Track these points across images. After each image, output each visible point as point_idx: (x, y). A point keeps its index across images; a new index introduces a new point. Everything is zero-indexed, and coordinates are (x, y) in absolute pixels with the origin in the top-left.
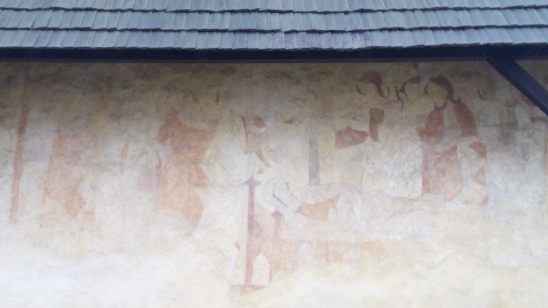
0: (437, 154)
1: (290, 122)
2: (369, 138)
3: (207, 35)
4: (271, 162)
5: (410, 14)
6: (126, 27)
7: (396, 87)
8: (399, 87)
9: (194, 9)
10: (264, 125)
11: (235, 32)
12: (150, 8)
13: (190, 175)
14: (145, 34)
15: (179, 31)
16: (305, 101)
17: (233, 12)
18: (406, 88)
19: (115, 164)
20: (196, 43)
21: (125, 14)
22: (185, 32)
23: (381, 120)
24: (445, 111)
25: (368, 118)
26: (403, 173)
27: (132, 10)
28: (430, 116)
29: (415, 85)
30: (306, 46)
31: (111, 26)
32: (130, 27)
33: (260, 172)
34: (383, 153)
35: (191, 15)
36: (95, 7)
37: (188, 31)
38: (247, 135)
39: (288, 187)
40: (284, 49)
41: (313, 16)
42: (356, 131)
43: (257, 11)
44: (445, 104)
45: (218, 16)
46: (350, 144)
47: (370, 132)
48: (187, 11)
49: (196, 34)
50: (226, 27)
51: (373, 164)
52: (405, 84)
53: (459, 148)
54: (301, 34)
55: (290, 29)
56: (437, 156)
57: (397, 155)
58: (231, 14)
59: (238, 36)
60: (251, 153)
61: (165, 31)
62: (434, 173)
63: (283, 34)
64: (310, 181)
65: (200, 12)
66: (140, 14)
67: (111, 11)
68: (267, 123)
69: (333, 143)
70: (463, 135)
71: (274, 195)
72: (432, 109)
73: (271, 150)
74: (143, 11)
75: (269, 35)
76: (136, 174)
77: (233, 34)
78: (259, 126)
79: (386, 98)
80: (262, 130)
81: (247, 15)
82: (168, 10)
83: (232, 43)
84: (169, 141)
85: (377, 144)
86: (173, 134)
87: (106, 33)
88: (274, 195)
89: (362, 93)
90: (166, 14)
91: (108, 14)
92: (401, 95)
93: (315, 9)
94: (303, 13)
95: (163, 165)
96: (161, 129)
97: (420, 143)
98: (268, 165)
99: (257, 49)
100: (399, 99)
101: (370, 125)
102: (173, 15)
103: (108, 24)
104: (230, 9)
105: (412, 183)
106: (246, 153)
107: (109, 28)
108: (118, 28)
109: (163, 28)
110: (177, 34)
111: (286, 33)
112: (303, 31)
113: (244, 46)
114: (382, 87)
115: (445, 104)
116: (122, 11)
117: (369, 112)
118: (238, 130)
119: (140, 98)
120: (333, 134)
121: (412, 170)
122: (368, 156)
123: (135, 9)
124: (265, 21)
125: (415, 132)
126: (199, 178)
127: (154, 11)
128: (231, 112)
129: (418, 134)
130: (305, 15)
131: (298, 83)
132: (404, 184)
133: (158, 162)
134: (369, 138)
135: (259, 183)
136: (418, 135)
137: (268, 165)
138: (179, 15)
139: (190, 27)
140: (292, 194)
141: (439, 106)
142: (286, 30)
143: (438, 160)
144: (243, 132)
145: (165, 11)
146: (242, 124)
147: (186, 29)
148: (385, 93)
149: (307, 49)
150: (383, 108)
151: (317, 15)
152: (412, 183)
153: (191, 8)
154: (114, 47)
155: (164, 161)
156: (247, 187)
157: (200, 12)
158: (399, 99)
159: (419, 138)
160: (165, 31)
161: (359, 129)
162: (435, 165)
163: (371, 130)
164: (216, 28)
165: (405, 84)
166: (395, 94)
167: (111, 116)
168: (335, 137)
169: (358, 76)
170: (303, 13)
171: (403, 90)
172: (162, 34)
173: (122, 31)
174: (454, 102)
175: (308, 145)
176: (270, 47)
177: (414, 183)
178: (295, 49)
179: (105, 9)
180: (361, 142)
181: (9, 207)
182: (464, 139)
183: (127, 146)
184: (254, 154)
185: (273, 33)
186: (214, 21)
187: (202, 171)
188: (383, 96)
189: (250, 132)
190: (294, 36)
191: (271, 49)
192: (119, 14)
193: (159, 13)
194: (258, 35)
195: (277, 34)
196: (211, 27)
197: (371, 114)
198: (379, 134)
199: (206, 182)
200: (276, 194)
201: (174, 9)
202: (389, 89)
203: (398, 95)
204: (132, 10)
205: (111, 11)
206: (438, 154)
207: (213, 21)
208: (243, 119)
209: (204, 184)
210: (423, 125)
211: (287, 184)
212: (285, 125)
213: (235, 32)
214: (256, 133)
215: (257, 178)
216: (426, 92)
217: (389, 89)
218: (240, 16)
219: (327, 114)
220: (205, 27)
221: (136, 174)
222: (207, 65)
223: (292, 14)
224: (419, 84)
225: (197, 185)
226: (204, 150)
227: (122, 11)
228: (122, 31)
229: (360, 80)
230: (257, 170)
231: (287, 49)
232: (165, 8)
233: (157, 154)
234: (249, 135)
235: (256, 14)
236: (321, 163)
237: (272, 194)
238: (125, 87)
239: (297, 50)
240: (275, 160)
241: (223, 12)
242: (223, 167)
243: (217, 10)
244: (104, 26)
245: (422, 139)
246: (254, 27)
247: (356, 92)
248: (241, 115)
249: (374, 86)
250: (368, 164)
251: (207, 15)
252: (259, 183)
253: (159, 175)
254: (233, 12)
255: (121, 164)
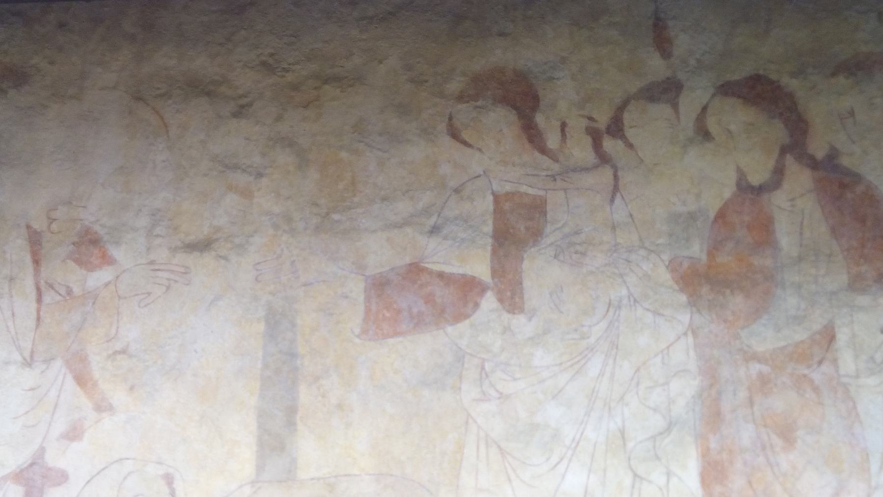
0: (755, 357)
1: (202, 246)
2: (489, 302)
4: (118, 396)
7: (591, 119)
8: (603, 120)
10: (107, 260)
16: (260, 175)
18: (628, 118)
23: (536, 234)
24: (779, 199)
25: (489, 228)
26: (622, 432)
28: (721, 216)
29: (661, 110)
33: (74, 434)
34: (541, 358)
38: (39, 300)
42: (441, 275)
44: (779, 173)
46: (418, 323)
47: (493, 277)
51: (503, 397)
52: (622, 108)
53: (842, 337)
56: (756, 368)
57: (595, 365)
62: (746, 434)
64: (260, 468)
68: (117, 253)
69: (354, 320)
70: (856, 284)
72: (728, 193)
78: (82, 262)
79: (556, 160)
80: (100, 277)
85: (518, 321)
89: (465, 143)
92: (609, 144)
97: (685, 317)
98: (103, 407)
100: (603, 158)
101: (494, 252)
105: (658, 477)
114: (540, 119)
115: (779, 173)
117: (491, 208)
120: (356, 288)
121: (657, 422)
122: (483, 368)
125: (664, 275)
129: (677, 282)
132: (628, 481)
134: (489, 302)
136: (676, 287)
137: (103, 407)
141: (756, 179)
143: (764, 384)
146: (28, 258)
148: (552, 141)
150: (541, 193)
152: (658, 477)
158: (603, 158)
159: (683, 298)
161: (454, 268)
162: (751, 402)
163: (497, 272)
165: (622, 108)
166: (588, 141)
168: (361, 298)
169: (454, 86)
171: (616, 129)
174: (814, 164)
175: (261, 327)
177: (669, 474)
180: (459, 317)
181: (34, 327)
182: (863, 300)
188: (543, 150)
189: (51, 286)
197: (498, 212)
198: (527, 283)
202: (563, 126)
203: (597, 145)
206: (759, 361)
208: (35, 241)
210: (697, 250)
212: (181, 258)
214: (77, 291)
215: (54, 459)
216: (704, 134)
217: (563, 126)
219: (336, 217)
224: (675, 106)
229: (461, 98)
230: (60, 426)
234: (47, 298)
236: (305, 395)
245: (694, 302)
247: (446, 140)
248: (28, 227)
249: (513, 116)
250: (484, 398)
252: (62, 477)
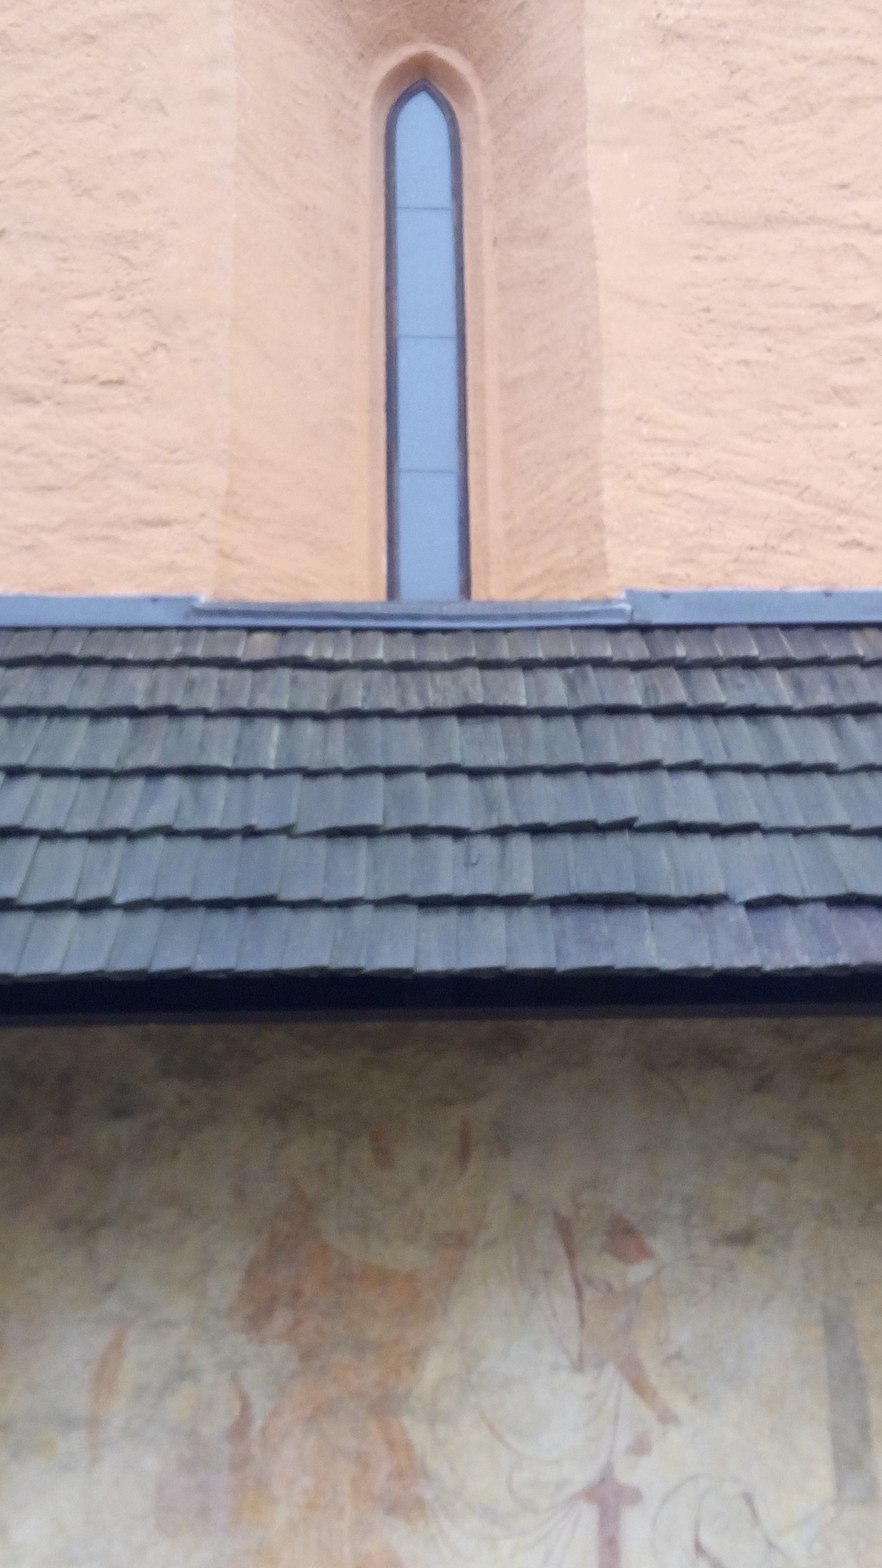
3: (451, 918)
4: (681, 1406)
5: (500, 783)
6: (147, 894)
9: (395, 823)
10: (645, 1253)
11: (557, 903)
12: (235, 823)
13: (363, 1462)
14: (221, 918)
15: (346, 904)
16: (793, 1159)
17: (538, 831)
19: (68, 1423)
20: (417, 952)
21: (142, 846)
22: (368, 909)
27: (169, 832)
30: (843, 958)
31: (92, 893)
32: (162, 893)
35: (385, 844)
36: (31, 823)
37: (381, 903)
38: (579, 1296)
39: (754, 1513)
40: (757, 969)
41: (838, 845)
43: (627, 826)
45: (487, 847)
48: (370, 832)
49: (411, 916)
50: (524, 885)
54: (809, 910)
55: (763, 891)
58: (531, 839)
59: (570, 919)
60: (600, 1365)
61: (295, 905)
63: (742, 911)
64: (840, 1487)
65: (419, 832)
66: (196, 843)
67: (92, 836)
68: (657, 1245)
71: (699, 1548)
73: (678, 1356)
74: (209, 834)
75: (686, 915)
76: (152, 1463)
77: (552, 914)
78: (623, 1256)
81: (591, 843)
82: (302, 828)
83: (552, 948)
84: (281, 1320)
86: (297, 1294)
87: (71, 920)
88: (699, 1548)
90: (293, 842)
91: (77, 848)
93: (840, 818)
94: (797, 832)
95: (258, 1423)
96: (250, 1273)
98: (667, 1418)
99: (652, 970)
102: (321, 846)
103: (80, 883)
104: (530, 819)
106: (579, 1366)
107: (83, 897)
108: (120, 899)
109: (284, 896)
110: (337, 915)
111: (751, 906)
112: (815, 900)
113: (602, 959)
116: (131, 835)
118: (547, 1273)
119: (175, 1153)
123: (178, 826)
124: (665, 861)
126: (399, 1474)
127: (250, 833)
128: (518, 1200)
130: (804, 839)
131: (761, 1086)
133: (237, 1412)
135: (635, 1496)
137: (667, 1418)
138: (342, 847)
139: (387, 891)
140: (770, 1545)
142: (751, 894)
144: (565, 1278)
145: (287, 831)
146: (561, 1250)
147: (371, 896)
149: (845, 967)
151: (852, 843)
153: (384, 819)
154: (101, 972)
155: (261, 1406)
156: (589, 1514)
157: (419, 832)
160: (295, 905)
164: (486, 888)
167: (63, 1225)
170: (797, 832)
172: (284, 916)
173: (133, 907)
175: (819, 1332)
176: (704, 964)
178: (803, 969)
179: (69, 829)
183: (117, 1345)
184: (610, 1370)
185: (703, 908)
186: (474, 865)
187: (408, 1447)
189: (590, 1281)
190: (787, 918)
191: (708, 969)
192: (119, 846)
193: (269, 839)
194: (644, 914)
195: (718, 912)
196: (465, 889)
199: (429, 1495)
200: (707, 1541)
201: (321, 825)
204: (169, 832)
205: (92, 836)
207: (469, 864)
209: (420, 1504)
211: (748, 1499)
212: (723, 1252)
213: (557, 903)
214: (617, 1285)
218: (565, 844)
220: (444, 887)
221: (152, 1463)
222: (422, 1027)
223: (757, 837)
225: (393, 1508)
226: (415, 1358)
227: (131, 835)
228: (133, 907)
230: (624, 1440)
231: (768, 967)
232: (291, 819)
233: (235, 1379)
234: (589, 1294)
235: (626, 838)
237: (690, 1546)
238: (120, 1113)
239: (808, 974)
240: (694, 1398)
241: (501, 832)
242: (491, 1427)
243: (479, 824)
244: (66, 892)
246: (629, 886)
248: (556, 1214)
251: (446, 846)
252: (635, 1496)
253: (239, 1464)
254: (538, 831)
255: (93, 1423)
